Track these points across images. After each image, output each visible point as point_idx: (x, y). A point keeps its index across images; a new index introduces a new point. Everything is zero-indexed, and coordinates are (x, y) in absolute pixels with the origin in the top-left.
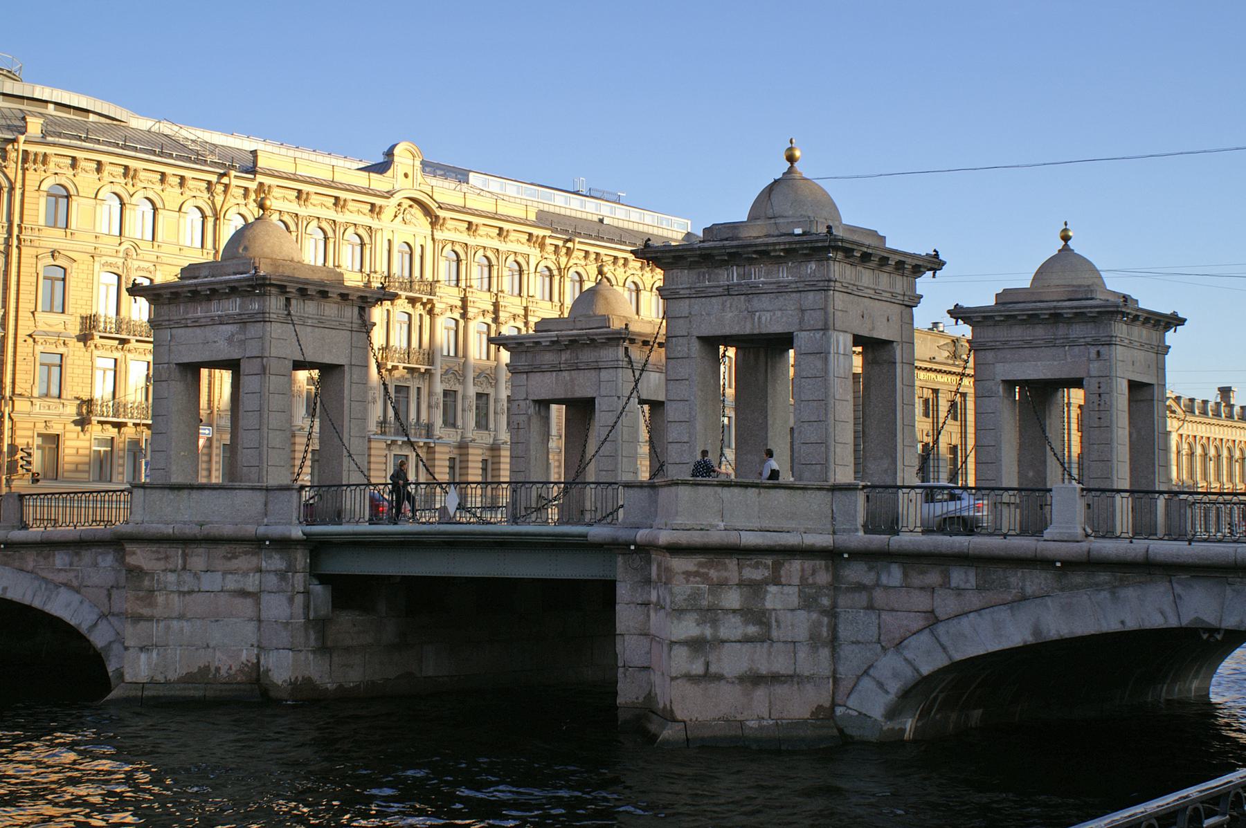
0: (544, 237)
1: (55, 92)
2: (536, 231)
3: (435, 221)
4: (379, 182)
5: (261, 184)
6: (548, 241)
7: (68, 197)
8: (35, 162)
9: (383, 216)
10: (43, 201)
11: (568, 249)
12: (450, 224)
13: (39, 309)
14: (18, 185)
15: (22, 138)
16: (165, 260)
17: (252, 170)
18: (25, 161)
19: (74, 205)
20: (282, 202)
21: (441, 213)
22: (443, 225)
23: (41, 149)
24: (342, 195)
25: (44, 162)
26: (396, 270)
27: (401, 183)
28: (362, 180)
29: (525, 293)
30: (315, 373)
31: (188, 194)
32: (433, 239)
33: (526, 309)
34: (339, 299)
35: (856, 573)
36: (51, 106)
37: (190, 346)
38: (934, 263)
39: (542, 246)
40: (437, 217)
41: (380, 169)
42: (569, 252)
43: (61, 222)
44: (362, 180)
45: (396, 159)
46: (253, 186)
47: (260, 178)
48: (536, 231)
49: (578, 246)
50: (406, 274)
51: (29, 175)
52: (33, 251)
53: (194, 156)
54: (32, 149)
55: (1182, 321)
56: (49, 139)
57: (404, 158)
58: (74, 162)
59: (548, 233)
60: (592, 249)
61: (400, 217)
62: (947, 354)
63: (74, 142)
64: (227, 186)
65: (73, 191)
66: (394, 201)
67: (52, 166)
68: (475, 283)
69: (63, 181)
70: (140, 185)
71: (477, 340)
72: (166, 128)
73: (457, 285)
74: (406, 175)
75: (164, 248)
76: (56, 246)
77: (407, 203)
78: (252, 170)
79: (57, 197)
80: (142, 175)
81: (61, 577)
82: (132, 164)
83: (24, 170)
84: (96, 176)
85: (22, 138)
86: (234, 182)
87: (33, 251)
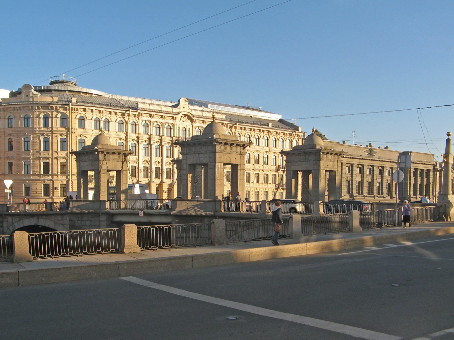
1: (90, 90)
2: (225, 122)
3: (192, 121)
4: (175, 110)
5: (139, 113)
6: (229, 125)
7: (109, 122)
8: (75, 110)
9: (176, 120)
11: (235, 127)
12: (197, 121)
13: (59, 150)
15: (70, 104)
16: (112, 136)
17: (136, 109)
18: (72, 110)
21: (194, 118)
22: (141, 115)
23: (76, 107)
25: (77, 110)
26: (181, 135)
27: (182, 110)
28: (170, 110)
29: (137, 132)
31: (246, 132)
32: (192, 126)
33: (138, 137)
36: (81, 93)
39: (227, 126)
40: (193, 120)
41: (176, 106)
42: (235, 128)
43: (107, 130)
44: (170, 110)
45: (180, 103)
46: (137, 113)
47: (139, 111)
48: (225, 122)
49: (238, 126)
50: (185, 137)
51: (73, 114)
52: (76, 135)
53: (120, 105)
54: (73, 107)
56: (78, 104)
57: (183, 102)
58: (85, 110)
59: (229, 122)
60: (243, 127)
61: (182, 120)
62: (367, 153)
64: (129, 115)
65: (110, 120)
66: (181, 115)
67: (79, 112)
68: (165, 134)
69: (108, 118)
70: (104, 115)
71: (144, 151)
72: (115, 97)
74: (184, 108)
75: (112, 133)
76: (81, 133)
77: (183, 116)
78: (136, 109)
79: (133, 125)
80: (104, 112)
81: (60, 222)
82: (278, 131)
83: (72, 113)
85: (70, 104)
86: (131, 113)
87: (76, 135)
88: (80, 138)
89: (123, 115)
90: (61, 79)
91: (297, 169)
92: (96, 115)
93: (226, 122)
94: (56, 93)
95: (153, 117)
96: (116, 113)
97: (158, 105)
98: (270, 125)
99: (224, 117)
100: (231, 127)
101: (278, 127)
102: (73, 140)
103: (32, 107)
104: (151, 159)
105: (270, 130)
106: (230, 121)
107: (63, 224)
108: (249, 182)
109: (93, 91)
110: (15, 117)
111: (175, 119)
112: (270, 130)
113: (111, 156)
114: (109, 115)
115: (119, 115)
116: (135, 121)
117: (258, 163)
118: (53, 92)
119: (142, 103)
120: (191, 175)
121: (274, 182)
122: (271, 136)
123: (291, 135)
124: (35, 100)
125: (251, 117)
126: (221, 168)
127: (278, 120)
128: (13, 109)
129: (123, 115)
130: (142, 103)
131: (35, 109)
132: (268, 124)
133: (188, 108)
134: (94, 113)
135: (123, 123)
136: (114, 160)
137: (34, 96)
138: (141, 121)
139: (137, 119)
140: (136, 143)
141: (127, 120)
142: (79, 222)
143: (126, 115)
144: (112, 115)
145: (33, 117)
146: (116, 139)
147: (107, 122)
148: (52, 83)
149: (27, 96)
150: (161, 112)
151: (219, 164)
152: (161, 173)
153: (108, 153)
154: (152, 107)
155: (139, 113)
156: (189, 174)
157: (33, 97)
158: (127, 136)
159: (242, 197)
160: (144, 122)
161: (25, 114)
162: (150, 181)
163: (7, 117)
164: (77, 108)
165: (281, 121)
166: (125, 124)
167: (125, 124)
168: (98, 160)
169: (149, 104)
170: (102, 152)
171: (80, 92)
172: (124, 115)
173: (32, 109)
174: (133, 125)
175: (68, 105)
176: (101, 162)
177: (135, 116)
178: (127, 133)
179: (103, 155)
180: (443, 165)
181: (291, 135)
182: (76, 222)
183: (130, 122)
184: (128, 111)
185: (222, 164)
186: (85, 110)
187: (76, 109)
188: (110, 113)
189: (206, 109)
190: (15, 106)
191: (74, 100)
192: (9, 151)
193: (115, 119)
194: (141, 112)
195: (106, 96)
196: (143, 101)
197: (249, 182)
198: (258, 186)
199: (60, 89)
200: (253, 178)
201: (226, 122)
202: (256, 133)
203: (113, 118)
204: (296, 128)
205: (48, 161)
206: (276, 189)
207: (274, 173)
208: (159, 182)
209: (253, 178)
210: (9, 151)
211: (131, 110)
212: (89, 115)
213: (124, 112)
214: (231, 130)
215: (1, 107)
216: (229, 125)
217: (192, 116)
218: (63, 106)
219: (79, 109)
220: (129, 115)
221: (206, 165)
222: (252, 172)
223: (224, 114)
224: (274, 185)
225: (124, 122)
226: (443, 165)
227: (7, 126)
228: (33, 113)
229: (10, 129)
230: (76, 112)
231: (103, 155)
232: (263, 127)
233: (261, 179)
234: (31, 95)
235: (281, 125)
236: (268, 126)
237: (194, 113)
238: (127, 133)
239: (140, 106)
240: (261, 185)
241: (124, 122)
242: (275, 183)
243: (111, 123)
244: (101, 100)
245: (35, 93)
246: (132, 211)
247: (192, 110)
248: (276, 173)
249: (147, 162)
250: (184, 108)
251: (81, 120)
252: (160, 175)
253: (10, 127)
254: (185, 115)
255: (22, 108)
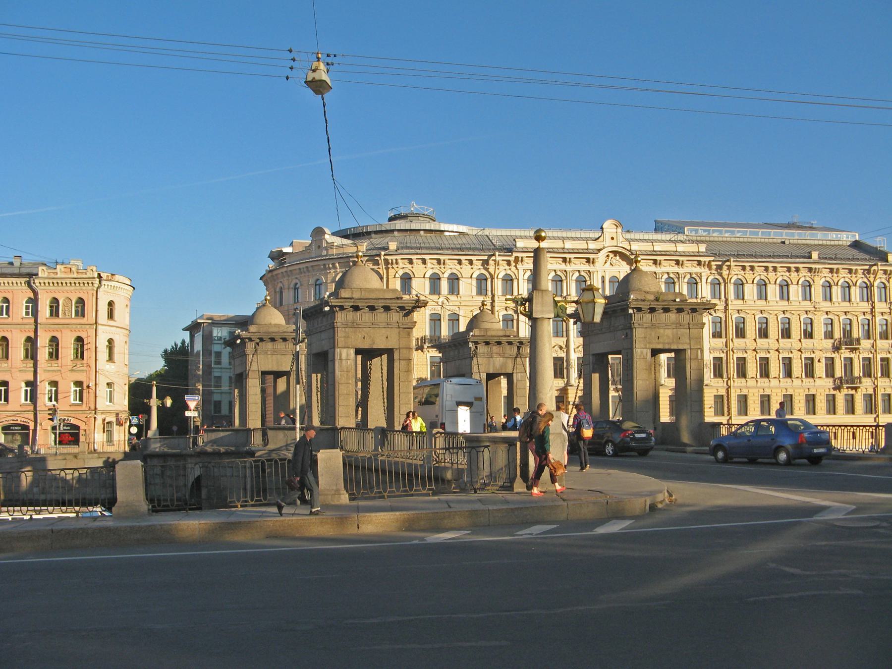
0: (710, 262)
1: (442, 225)
5: (517, 258)
6: (713, 263)
9: (596, 264)
10: (858, 290)
14: (385, 277)
19: (813, 289)
20: (645, 266)
22: (522, 261)
24: (568, 256)
25: (397, 263)
30: (673, 355)
34: (367, 309)
35: (171, 462)
36: (422, 232)
37: (599, 348)
39: (709, 266)
46: (512, 259)
47: (515, 254)
51: (391, 270)
56: (399, 252)
60: (747, 264)
61: (608, 263)
63: (785, 260)
64: (729, 267)
67: (401, 265)
73: (886, 301)
74: (612, 238)
75: (463, 298)
77: (611, 255)
80: (447, 261)
82: (442, 257)
83: (387, 269)
84: (470, 267)
88: (505, 312)
89: (485, 263)
90: (403, 211)
91: (602, 350)
92: (431, 268)
93: (707, 259)
94: (379, 236)
95: (570, 262)
96: (471, 262)
97: (577, 239)
98: (815, 255)
99: (703, 248)
100: (719, 268)
101: (853, 259)
103: (324, 265)
104: (568, 341)
105: (813, 266)
106: (715, 255)
108: (767, 376)
109: (443, 227)
110: (301, 285)
111: (593, 263)
112: (813, 266)
113: (270, 345)
114: (458, 267)
115: (478, 264)
116: (509, 272)
117: (789, 337)
118: (373, 235)
119: (521, 237)
120: (319, 375)
121: (830, 372)
122: (816, 279)
123: (869, 271)
124: (330, 252)
125: (784, 243)
126: (347, 359)
127: (849, 243)
128: (298, 271)
129: (485, 263)
130: (521, 237)
131: (330, 269)
132: (810, 253)
133: (621, 239)
134: (429, 265)
135: (719, 284)
136: (274, 352)
137: (331, 245)
138: (521, 272)
139: (513, 268)
140: (512, 313)
141: (726, 277)
143: (725, 268)
144: (464, 266)
145: (326, 282)
146: (472, 308)
147: (454, 280)
148: (391, 219)
149: (319, 247)
150: (653, 253)
151: (344, 351)
152: (567, 368)
153: (261, 340)
154: (569, 245)
155: (517, 258)
156: (314, 375)
157: (326, 249)
158: (727, 305)
160: (689, 276)
161: (315, 278)
162: (568, 384)
163: (292, 286)
164: (838, 269)
165: (856, 245)
166: (489, 280)
167: (489, 280)
168: (244, 355)
169: (563, 239)
170: (250, 340)
171: (419, 230)
172: (721, 269)
173: (325, 269)
175: (379, 255)
176: (249, 358)
177: (509, 263)
178: (727, 300)
179: (253, 344)
180: (327, 309)
181: (869, 273)
183: (732, 281)
184: (728, 261)
185: (352, 352)
186: (411, 262)
187: (394, 261)
188: (744, 268)
189: (681, 237)
190: (301, 266)
191: (393, 246)
193: (469, 273)
194: (520, 255)
195: (471, 233)
196: (523, 233)
197: (767, 376)
198: (767, 384)
200: (752, 368)
201: (707, 259)
202: (801, 275)
203: (466, 270)
204: (882, 257)
206: (834, 389)
207: (829, 355)
208: (563, 385)
209: (752, 368)
211: (497, 253)
212: (418, 269)
213: (486, 258)
214: (721, 275)
216: (713, 263)
217: (628, 253)
218: (372, 258)
219: (400, 261)
220: (497, 263)
221: (390, 352)
222: (795, 356)
224: (831, 380)
225: (721, 281)
226: (327, 309)
228: (326, 275)
230: (395, 266)
231: (253, 344)
232: (798, 260)
233: (798, 368)
234: (325, 245)
235: (855, 252)
236: (810, 257)
237: (635, 247)
238: (727, 300)
239: (520, 244)
240: (751, 383)
241: (721, 281)
242: (833, 376)
243: (769, 287)
244: (464, 240)
245: (338, 241)
247: (629, 241)
248: (833, 355)
249: (561, 348)
250: (612, 238)
251: (481, 280)
252: (565, 371)
254: (615, 253)
255: (310, 269)
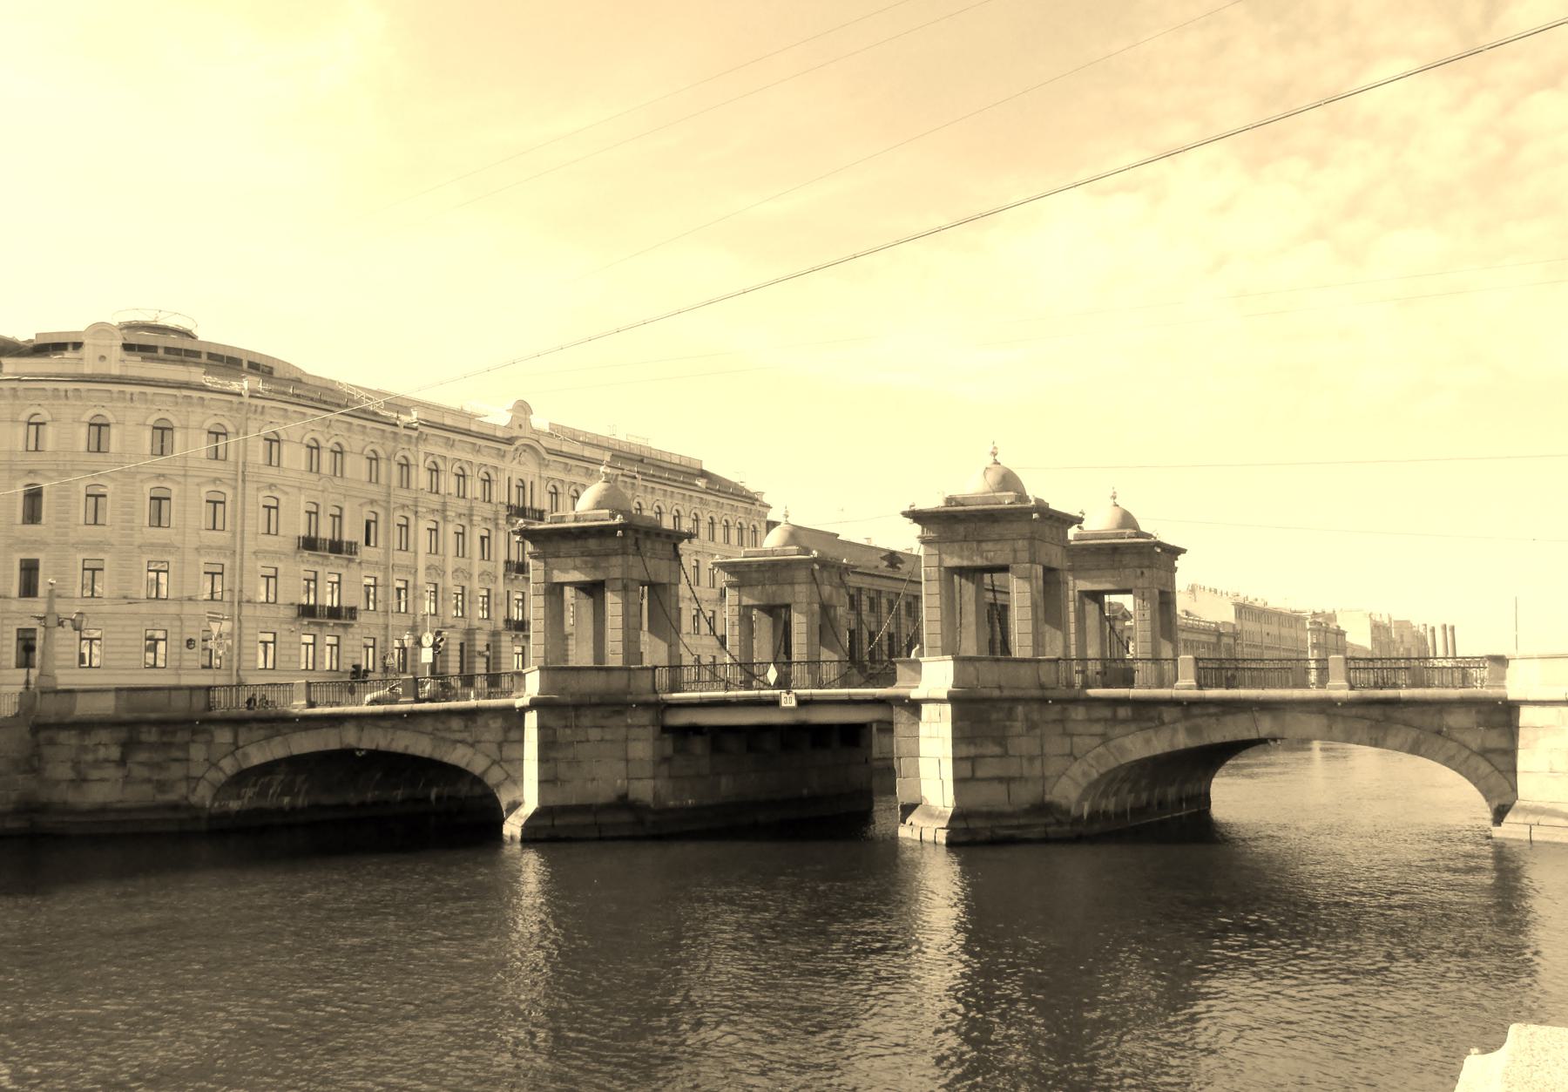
25: (262, 413)
38: (1080, 520)
55: (1184, 551)
81: (458, 736)
102: (1537, 708)
107: (470, 740)
142: (568, 731)
147: (339, 452)
158: (389, 495)
159: (687, 660)
163: (24, 417)
174: (371, 459)
182: (560, 732)
192: (24, 523)
199: (565, 449)
205: (1313, 677)
210: (24, 523)
215: (5, 385)
223: (609, 449)
227: (21, 447)
229: (35, 457)
246: (388, 708)
253: (32, 447)
